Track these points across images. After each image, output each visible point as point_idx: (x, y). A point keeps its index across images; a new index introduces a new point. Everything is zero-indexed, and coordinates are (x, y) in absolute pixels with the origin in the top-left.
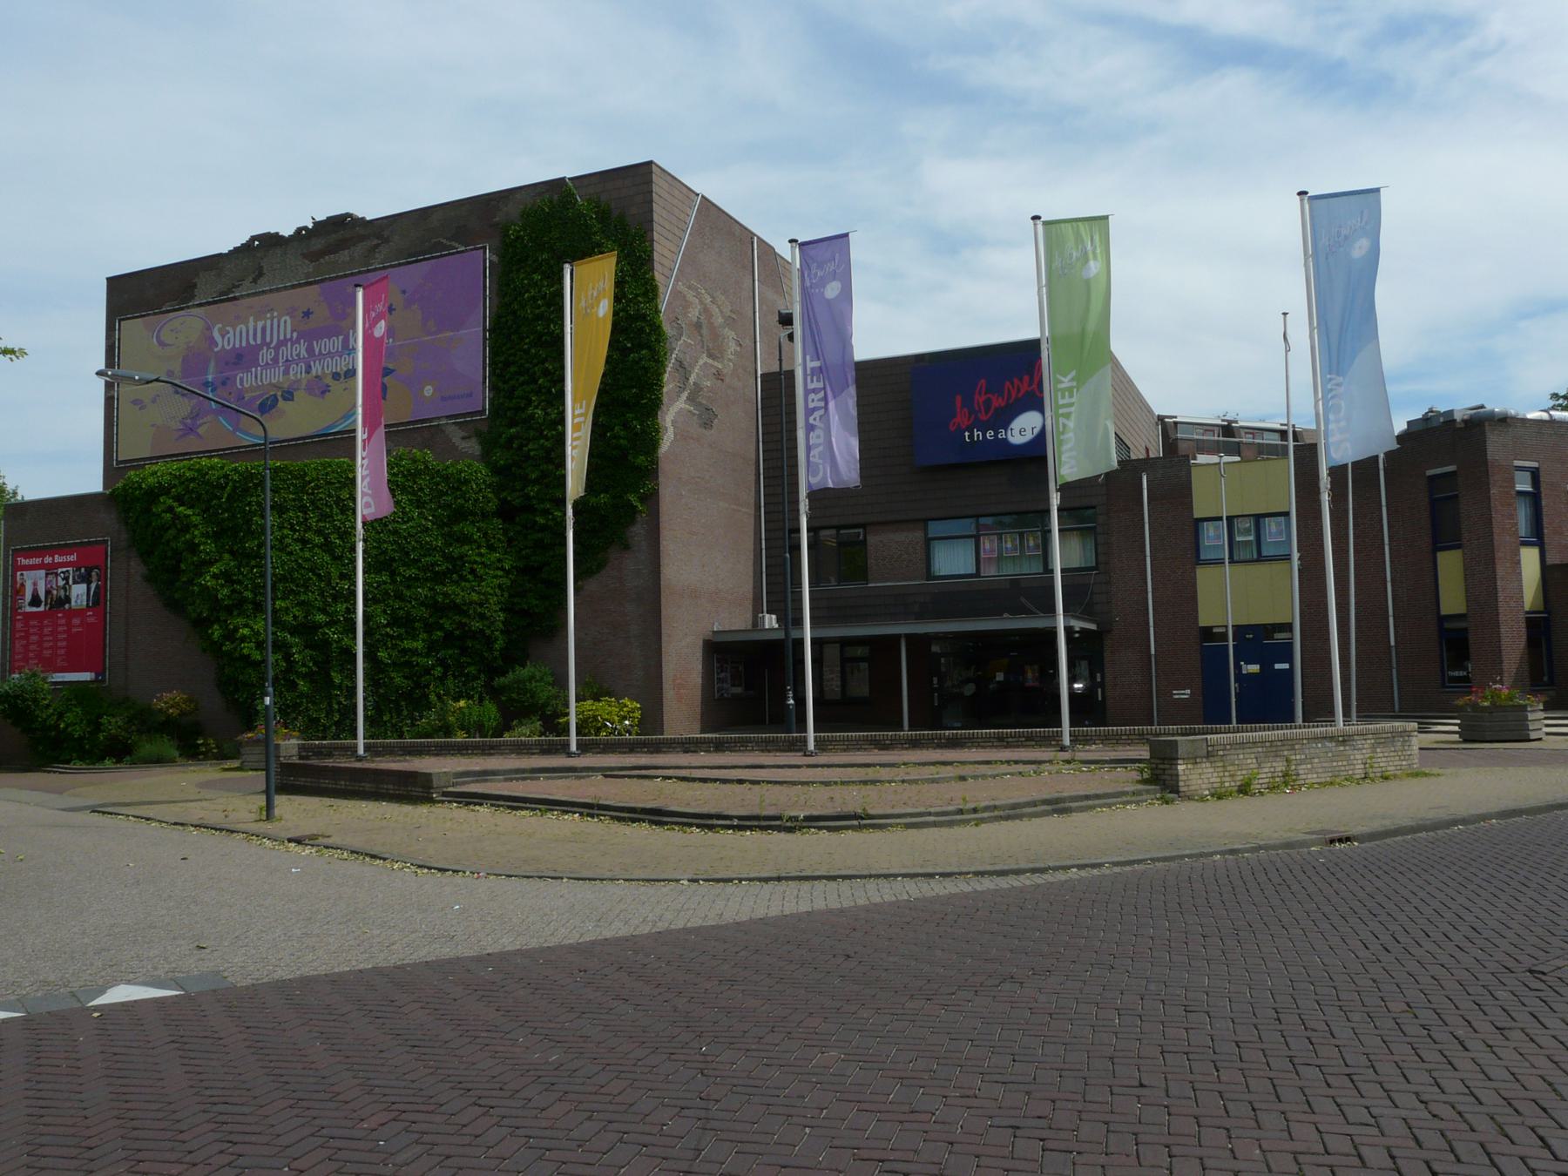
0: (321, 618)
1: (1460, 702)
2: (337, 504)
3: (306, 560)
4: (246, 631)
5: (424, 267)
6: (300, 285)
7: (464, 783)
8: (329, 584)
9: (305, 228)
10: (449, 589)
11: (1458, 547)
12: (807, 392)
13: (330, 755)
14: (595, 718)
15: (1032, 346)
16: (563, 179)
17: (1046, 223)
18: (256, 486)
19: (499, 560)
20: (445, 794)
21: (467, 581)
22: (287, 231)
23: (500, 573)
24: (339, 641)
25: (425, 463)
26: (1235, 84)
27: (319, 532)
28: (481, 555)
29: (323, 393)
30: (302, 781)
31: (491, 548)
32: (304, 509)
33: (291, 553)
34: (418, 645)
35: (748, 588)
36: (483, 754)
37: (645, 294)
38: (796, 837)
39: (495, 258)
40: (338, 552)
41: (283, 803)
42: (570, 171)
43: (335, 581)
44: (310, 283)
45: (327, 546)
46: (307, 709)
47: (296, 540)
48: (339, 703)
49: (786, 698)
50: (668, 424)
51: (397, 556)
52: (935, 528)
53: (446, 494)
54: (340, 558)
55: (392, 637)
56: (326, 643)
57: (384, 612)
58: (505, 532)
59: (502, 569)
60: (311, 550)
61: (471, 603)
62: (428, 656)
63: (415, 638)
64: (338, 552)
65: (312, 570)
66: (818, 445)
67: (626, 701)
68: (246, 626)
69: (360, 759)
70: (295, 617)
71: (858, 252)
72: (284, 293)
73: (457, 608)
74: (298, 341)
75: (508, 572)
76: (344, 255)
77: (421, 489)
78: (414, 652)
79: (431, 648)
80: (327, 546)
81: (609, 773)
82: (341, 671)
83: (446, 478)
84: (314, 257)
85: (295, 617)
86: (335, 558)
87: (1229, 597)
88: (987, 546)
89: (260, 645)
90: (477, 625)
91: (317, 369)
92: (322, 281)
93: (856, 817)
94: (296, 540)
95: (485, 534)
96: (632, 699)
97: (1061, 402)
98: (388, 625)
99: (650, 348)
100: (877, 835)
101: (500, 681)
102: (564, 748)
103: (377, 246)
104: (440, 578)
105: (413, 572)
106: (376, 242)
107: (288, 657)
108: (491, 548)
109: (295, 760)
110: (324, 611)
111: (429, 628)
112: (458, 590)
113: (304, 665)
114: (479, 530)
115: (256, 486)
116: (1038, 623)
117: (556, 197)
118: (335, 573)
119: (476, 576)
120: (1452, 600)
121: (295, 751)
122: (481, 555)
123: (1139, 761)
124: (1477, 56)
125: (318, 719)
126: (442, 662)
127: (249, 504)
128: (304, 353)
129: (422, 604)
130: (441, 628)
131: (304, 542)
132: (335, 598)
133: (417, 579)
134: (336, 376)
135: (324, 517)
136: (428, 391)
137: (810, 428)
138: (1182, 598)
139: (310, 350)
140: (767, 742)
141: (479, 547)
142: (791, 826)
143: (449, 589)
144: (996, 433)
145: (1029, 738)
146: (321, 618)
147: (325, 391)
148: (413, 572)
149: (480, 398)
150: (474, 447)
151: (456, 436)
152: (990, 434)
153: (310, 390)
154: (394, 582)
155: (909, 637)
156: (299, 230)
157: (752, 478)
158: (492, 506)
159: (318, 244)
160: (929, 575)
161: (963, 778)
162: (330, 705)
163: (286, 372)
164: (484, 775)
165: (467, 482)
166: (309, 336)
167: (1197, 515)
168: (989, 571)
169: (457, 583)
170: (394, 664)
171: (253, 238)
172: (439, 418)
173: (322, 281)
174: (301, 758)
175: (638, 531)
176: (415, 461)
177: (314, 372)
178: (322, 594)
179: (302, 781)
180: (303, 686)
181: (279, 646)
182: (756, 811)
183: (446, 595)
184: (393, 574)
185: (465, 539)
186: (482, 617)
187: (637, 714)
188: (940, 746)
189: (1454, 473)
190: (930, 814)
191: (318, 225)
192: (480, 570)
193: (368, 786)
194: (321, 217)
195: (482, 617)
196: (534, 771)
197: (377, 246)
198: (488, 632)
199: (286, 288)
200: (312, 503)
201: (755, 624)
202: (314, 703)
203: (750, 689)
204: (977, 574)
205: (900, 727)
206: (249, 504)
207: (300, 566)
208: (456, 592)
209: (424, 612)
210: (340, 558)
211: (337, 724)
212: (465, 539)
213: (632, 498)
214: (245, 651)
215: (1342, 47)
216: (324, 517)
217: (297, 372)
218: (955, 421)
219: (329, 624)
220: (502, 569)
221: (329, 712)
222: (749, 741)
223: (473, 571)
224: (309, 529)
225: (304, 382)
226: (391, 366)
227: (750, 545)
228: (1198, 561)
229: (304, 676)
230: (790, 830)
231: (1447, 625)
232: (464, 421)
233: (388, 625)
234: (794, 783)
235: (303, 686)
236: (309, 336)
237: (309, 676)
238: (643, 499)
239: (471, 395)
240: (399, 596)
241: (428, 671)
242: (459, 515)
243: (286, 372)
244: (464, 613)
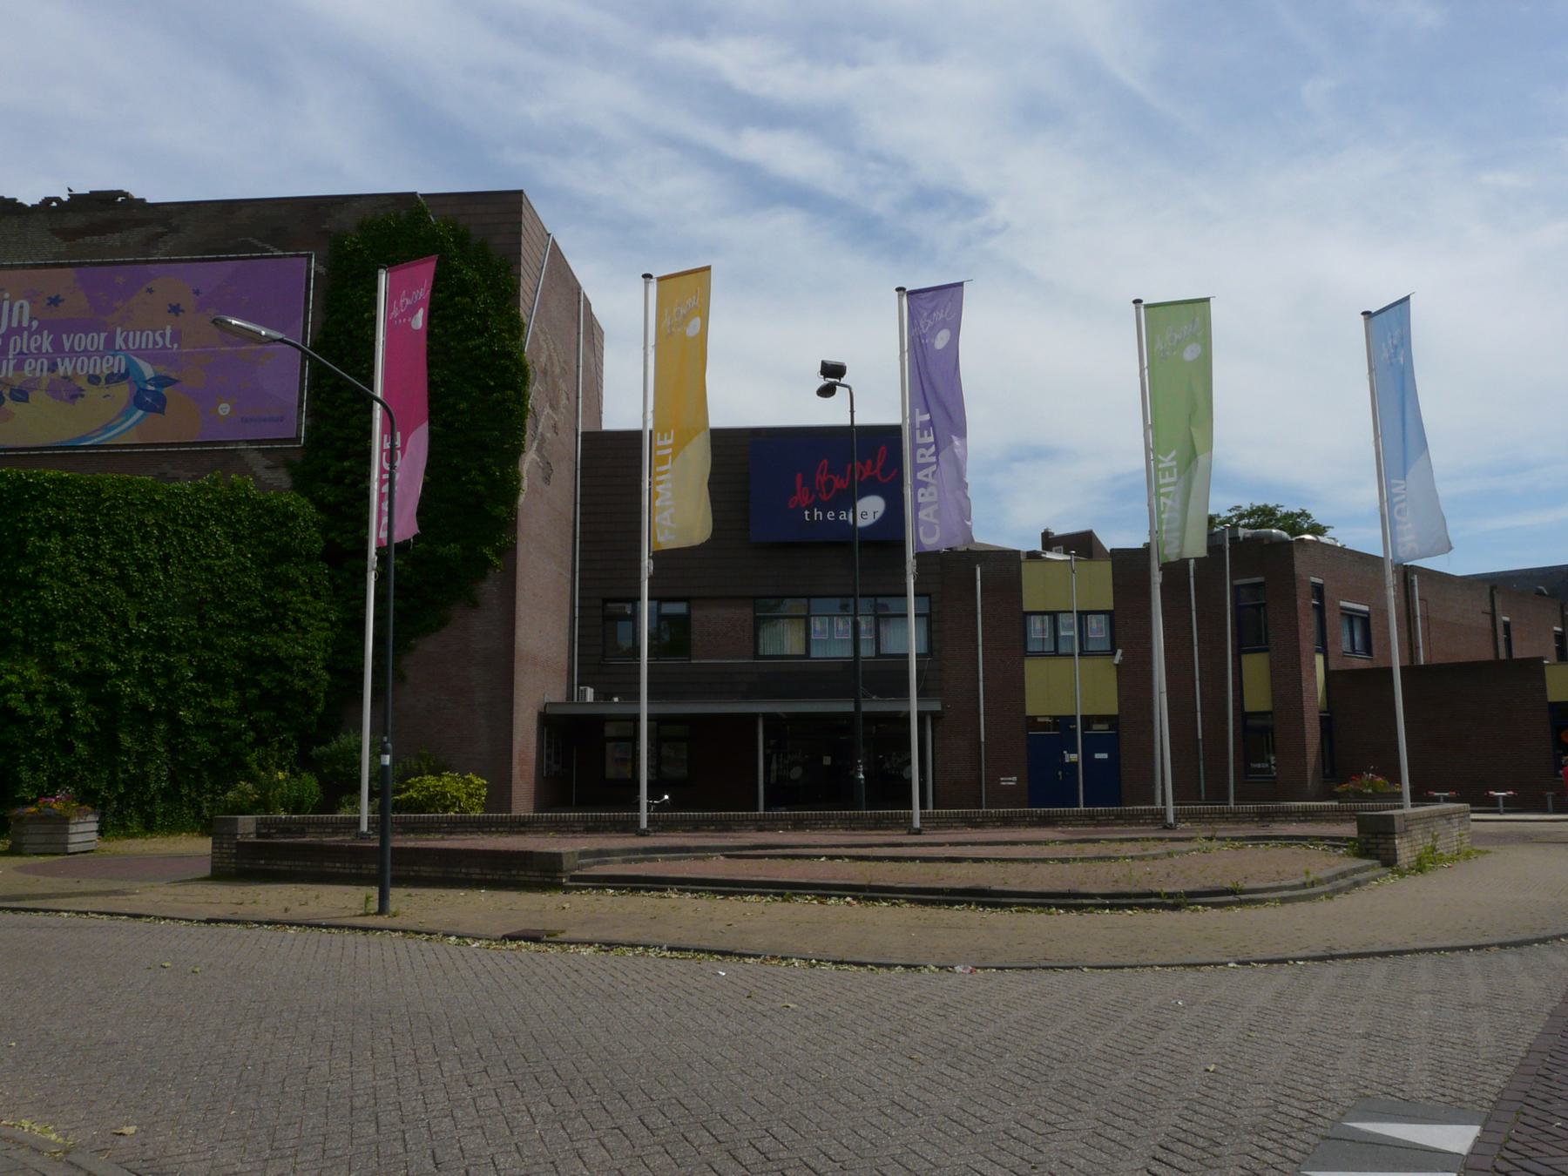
0: (112, 666)
1: (1338, 789)
2: (138, 529)
3: (96, 594)
4: (14, 678)
5: (228, 267)
6: (46, 266)
7: (589, 865)
8: (125, 625)
9: (57, 199)
10: (270, 640)
11: (1266, 650)
12: (915, 447)
13: (303, 833)
14: (444, 795)
15: (895, 431)
16: (414, 194)
17: (1147, 306)
18: (34, 499)
19: (325, 611)
20: (573, 878)
21: (289, 631)
22: (30, 196)
23: (327, 625)
24: (132, 695)
25: (247, 490)
26: (787, 224)
27: (113, 562)
28: (305, 602)
29: (74, 397)
30: (284, 865)
31: (316, 596)
32: (95, 533)
33: (76, 585)
34: (229, 703)
35: (563, 659)
36: (558, 832)
37: (510, 331)
38: (1185, 915)
39: (322, 270)
40: (136, 587)
41: (397, 895)
42: (422, 188)
43: (132, 623)
44: (61, 266)
45: (123, 580)
46: (82, 779)
47: (82, 570)
48: (127, 771)
49: (857, 773)
50: (524, 474)
51: (209, 596)
52: (816, 603)
53: (269, 529)
54: (139, 595)
55: (196, 694)
56: (115, 697)
57: (190, 662)
58: (332, 579)
59: (327, 620)
60: (101, 582)
61: (296, 658)
62: (239, 717)
63: (223, 695)
64: (136, 587)
65: (102, 608)
66: (930, 504)
67: (471, 776)
68: (11, 672)
69: (363, 836)
70: (78, 663)
71: (1216, 311)
72: (19, 272)
73: (278, 663)
74: (39, 331)
75: (333, 624)
76: (115, 239)
77: (239, 521)
78: (222, 712)
79: (244, 708)
80: (123, 580)
81: (732, 853)
82: (131, 733)
83: (270, 511)
84: (70, 235)
85: (78, 663)
86: (130, 594)
87: (1070, 687)
88: (818, 627)
89: (30, 697)
90: (300, 684)
91: (65, 367)
92: (80, 265)
93: (1233, 892)
94: (82, 570)
95: (311, 579)
96: (478, 775)
97: (1162, 481)
98: (192, 679)
99: (514, 389)
100: (1250, 912)
101: (316, 751)
102: (906, 824)
103: (162, 235)
104: (256, 626)
105: (225, 617)
106: (159, 230)
107: (66, 713)
108: (316, 596)
109: (252, 838)
110: (114, 658)
111: (241, 684)
112: (280, 642)
113: (85, 723)
114: (304, 573)
115: (34, 499)
116: (627, 709)
117: (403, 212)
118: (132, 615)
119: (299, 627)
120: (1258, 698)
121: (252, 828)
122: (305, 602)
123: (1349, 839)
124: (988, 232)
125: (97, 792)
126: (253, 725)
127: (23, 520)
128: (46, 347)
129: (236, 656)
130: (257, 684)
131: (93, 572)
132: (129, 643)
133: (230, 626)
134: (94, 380)
135: (121, 544)
136: (224, 409)
137: (918, 484)
138: (1010, 687)
139: (57, 345)
140: (851, 819)
141: (303, 594)
142: (1175, 902)
143: (270, 640)
144: (837, 515)
145: (1119, 816)
146: (112, 666)
147: (75, 395)
148: (225, 617)
149: (297, 426)
150: (282, 478)
151: (259, 464)
152: (830, 515)
153: (53, 391)
154: (202, 627)
155: (766, 716)
156: (48, 201)
157: (570, 541)
158: (318, 547)
159: (75, 221)
160: (756, 655)
161: (1170, 855)
162: (113, 774)
163: (19, 367)
164: (601, 855)
165: (294, 517)
166: (58, 328)
167: (1027, 607)
168: (816, 652)
169: (275, 632)
170: (198, 726)
171: (121, 193)
172: (236, 442)
173: (80, 265)
174: (259, 835)
175: (488, 588)
176: (232, 487)
177: (61, 371)
178: (114, 637)
179: (284, 865)
180: (81, 748)
181: (53, 699)
182: (1147, 888)
183: (265, 647)
184: (201, 618)
185: (291, 584)
186: (306, 675)
187: (484, 792)
188: (1032, 824)
189: (1261, 584)
190: (1285, 888)
191: (74, 198)
192: (304, 621)
193: (476, 873)
194: (83, 188)
195: (306, 675)
196: (647, 850)
197: (162, 235)
198: (311, 692)
199: (24, 266)
200: (107, 526)
201: (570, 696)
202: (93, 772)
203: (583, 765)
204: (807, 655)
205: (1225, 800)
206: (23, 520)
207: (88, 601)
208: (283, 646)
209: (236, 666)
210: (139, 595)
211: (120, 798)
212: (291, 584)
213: (487, 551)
214: (12, 704)
215: (880, 205)
216: (121, 544)
217: (34, 369)
218: (812, 500)
219: (120, 675)
220: (327, 620)
221: (112, 784)
222: (830, 818)
223: (296, 621)
224: (99, 557)
225: (45, 383)
226: (174, 376)
227: (567, 613)
228: (1026, 653)
229: (82, 737)
230: (1176, 907)
231: (1250, 722)
232: (272, 450)
233: (192, 679)
234: (1044, 861)
235: (81, 748)
236: (58, 328)
237: (89, 738)
238: (499, 553)
239: (282, 419)
240: (208, 645)
241: (238, 735)
242: (284, 554)
243: (19, 367)
244: (289, 670)
